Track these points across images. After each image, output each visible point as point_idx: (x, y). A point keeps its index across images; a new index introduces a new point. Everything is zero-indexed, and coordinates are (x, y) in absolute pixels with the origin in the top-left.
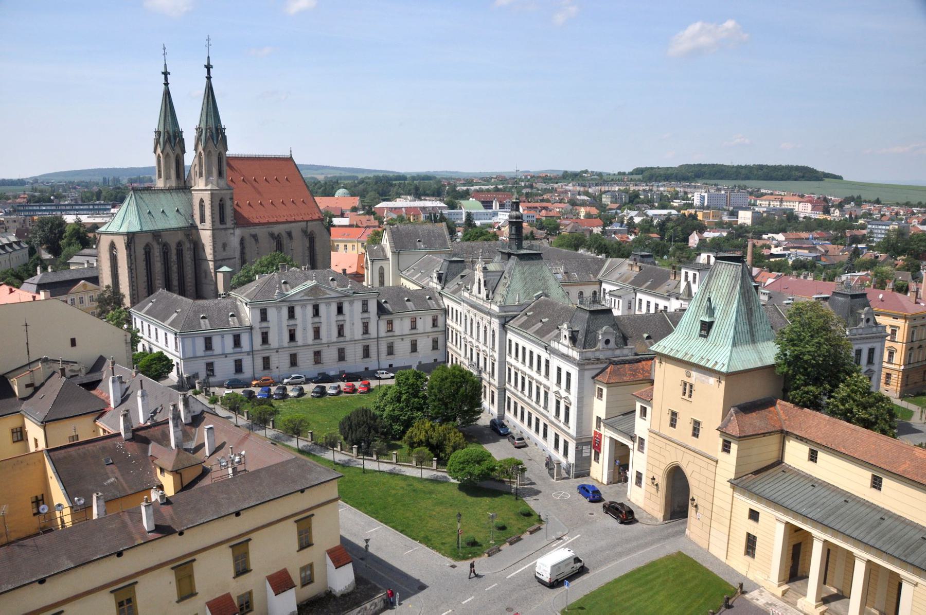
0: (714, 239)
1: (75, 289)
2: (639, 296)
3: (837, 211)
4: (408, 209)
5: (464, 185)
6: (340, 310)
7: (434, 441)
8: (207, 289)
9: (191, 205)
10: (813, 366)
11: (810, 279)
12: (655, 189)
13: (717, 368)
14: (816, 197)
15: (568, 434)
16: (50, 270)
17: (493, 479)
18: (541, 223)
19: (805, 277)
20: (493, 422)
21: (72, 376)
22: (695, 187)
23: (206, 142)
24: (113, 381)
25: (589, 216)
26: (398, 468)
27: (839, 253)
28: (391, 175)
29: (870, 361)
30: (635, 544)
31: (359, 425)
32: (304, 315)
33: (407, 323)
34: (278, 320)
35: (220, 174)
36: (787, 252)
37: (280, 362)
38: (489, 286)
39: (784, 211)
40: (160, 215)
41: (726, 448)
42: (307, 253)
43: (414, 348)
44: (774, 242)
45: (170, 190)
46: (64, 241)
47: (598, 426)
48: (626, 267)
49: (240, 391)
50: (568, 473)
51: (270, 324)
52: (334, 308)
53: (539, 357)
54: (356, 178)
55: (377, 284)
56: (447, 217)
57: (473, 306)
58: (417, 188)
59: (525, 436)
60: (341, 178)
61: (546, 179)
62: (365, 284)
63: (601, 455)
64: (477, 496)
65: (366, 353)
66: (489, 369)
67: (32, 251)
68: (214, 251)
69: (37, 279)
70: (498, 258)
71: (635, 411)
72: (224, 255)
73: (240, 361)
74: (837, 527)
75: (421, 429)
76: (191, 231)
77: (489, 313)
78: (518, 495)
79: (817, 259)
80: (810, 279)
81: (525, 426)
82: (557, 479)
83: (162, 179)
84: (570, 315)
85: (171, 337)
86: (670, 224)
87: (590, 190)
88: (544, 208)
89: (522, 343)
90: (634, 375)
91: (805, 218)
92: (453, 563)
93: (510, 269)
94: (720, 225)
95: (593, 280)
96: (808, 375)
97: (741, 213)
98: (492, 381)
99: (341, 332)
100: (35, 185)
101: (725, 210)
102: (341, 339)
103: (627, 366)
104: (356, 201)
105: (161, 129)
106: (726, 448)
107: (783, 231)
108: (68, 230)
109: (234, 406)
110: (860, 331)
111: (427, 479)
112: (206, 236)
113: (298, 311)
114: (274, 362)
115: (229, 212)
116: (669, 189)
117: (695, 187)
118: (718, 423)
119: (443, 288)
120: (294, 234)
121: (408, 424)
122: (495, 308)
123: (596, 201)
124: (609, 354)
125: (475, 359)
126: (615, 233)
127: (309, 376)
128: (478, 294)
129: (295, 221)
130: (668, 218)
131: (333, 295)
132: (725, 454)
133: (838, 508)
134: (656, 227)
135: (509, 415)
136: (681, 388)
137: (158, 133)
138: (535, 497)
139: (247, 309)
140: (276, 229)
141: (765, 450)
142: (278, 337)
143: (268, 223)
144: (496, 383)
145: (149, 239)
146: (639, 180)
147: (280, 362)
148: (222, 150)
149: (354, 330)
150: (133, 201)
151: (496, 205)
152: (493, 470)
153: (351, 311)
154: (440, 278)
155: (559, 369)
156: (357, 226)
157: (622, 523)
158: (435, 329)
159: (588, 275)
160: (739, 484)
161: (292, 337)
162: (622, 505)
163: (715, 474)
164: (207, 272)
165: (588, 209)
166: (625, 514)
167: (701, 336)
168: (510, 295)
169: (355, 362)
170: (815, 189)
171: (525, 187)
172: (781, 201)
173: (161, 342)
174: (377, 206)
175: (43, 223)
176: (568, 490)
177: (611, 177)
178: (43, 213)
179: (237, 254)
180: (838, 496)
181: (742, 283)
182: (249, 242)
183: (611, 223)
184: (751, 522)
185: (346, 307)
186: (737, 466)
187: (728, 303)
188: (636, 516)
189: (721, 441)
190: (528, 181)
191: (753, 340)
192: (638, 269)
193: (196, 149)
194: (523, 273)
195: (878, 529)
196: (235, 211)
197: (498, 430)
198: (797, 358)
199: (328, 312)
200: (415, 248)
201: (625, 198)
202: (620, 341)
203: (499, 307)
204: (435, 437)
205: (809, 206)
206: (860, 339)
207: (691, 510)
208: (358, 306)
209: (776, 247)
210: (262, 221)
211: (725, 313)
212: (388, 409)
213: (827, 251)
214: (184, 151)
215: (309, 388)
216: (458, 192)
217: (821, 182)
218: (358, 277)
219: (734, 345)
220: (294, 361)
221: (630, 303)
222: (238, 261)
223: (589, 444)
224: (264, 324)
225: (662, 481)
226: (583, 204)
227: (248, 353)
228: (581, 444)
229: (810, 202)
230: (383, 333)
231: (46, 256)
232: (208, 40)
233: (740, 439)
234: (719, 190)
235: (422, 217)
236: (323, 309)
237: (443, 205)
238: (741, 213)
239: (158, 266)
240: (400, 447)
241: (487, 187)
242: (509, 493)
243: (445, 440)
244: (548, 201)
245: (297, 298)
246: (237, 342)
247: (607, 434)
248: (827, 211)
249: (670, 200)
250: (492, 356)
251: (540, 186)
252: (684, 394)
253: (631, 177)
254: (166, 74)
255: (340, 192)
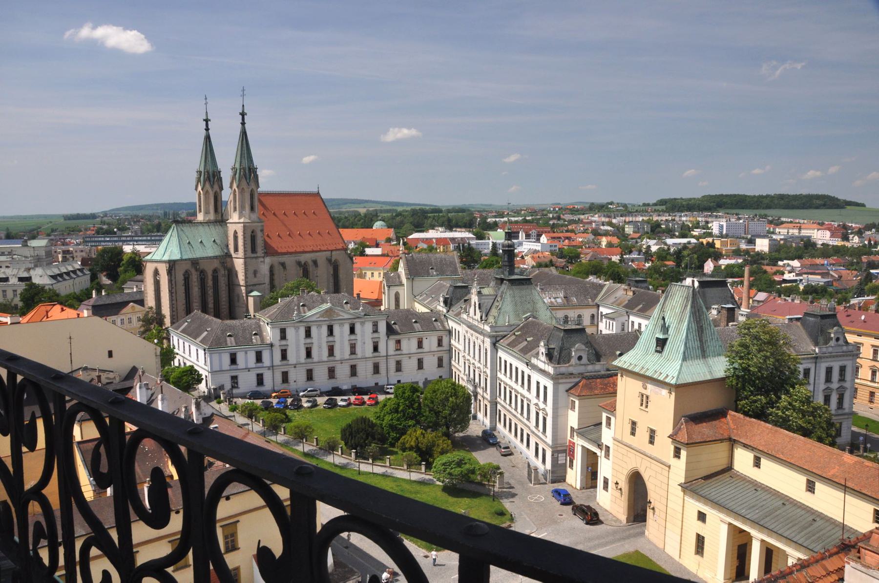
0: (728, 266)
1: (124, 311)
2: (632, 318)
3: (856, 237)
4: (439, 241)
5: (495, 217)
6: (352, 331)
7: (423, 447)
8: (239, 311)
9: (227, 237)
10: (758, 378)
11: (797, 301)
12: (677, 219)
13: (667, 380)
14: (836, 224)
15: (545, 442)
16: (103, 294)
17: (472, 482)
18: (562, 252)
19: (793, 300)
20: (484, 432)
21: (108, 383)
22: (716, 216)
23: (240, 180)
24: (140, 388)
25: (610, 245)
26: (390, 471)
27: (852, 278)
28: (427, 208)
29: (842, 378)
30: (596, 542)
31: (358, 432)
32: (319, 334)
33: (414, 343)
34: (295, 336)
35: (252, 208)
36: (798, 278)
37: (297, 377)
38: (484, 309)
39: (802, 238)
40: (199, 245)
41: (677, 454)
42: (332, 280)
43: (420, 363)
44: (789, 268)
45: (208, 223)
46: (122, 268)
47: (572, 436)
48: (623, 293)
49: (258, 402)
50: (546, 479)
51: (289, 343)
52: (347, 328)
53: (523, 372)
54: (396, 211)
55: (393, 307)
56: (474, 246)
57: (471, 327)
58: (449, 220)
59: (512, 445)
60: (381, 211)
61: (574, 211)
62: (383, 308)
63: (575, 462)
64: (457, 497)
65: (376, 369)
66: (483, 384)
67: (94, 277)
68: (246, 277)
69: (92, 302)
70: (492, 284)
71: (601, 423)
72: (255, 281)
73: (262, 375)
74: (770, 528)
75: (414, 435)
76: (226, 258)
77: (482, 333)
78: (496, 497)
79: (829, 284)
80: (797, 301)
81: (512, 436)
82: (535, 484)
83: (202, 213)
84: (548, 334)
85: (201, 352)
86: (685, 253)
87: (614, 221)
88: (567, 238)
89: (510, 360)
90: (605, 389)
91: (822, 245)
92: (427, 553)
93: (502, 292)
94: (737, 253)
95: (591, 303)
96: (754, 385)
97: (759, 241)
98: (485, 395)
99: (353, 351)
100: (105, 218)
101: (743, 238)
102: (353, 356)
103: (598, 380)
104: (391, 233)
105: (202, 169)
106: (677, 454)
107: (799, 258)
108: (125, 258)
109: (251, 413)
110: (830, 349)
111: (415, 481)
112: (239, 264)
113: (314, 331)
114: (292, 377)
115: (259, 242)
116: (691, 219)
117: (716, 216)
118: (670, 431)
119: (448, 311)
120: (319, 262)
121: (403, 432)
122: (487, 328)
123: (619, 231)
124: (581, 369)
125: (472, 376)
126: (633, 261)
127: (323, 390)
128: (474, 315)
129: (320, 251)
130: (685, 247)
131: (346, 316)
132: (676, 459)
133: (776, 509)
134: (673, 255)
135: (500, 426)
136: (639, 399)
137: (200, 173)
138: (511, 500)
139: (268, 328)
140: (303, 258)
141: (715, 456)
142: (296, 354)
143: (296, 253)
144: (488, 397)
145: (188, 266)
146: (663, 211)
147: (297, 377)
148: (253, 186)
149: (365, 349)
150: (175, 233)
151: (522, 235)
152: (473, 472)
153: (363, 332)
154: (446, 302)
155: (538, 383)
156: (388, 256)
157: (587, 524)
158: (441, 348)
159: (586, 299)
160: (690, 487)
161: (309, 354)
162: (589, 507)
163: (667, 478)
164: (239, 296)
165: (610, 238)
166: (591, 516)
167: (657, 351)
168: (501, 316)
169: (365, 378)
170: (835, 218)
171: (553, 218)
172: (800, 229)
173: (193, 358)
174: (410, 237)
175: (105, 251)
176: (543, 495)
177: (636, 208)
178: (107, 243)
179: (267, 280)
180: (778, 499)
181: (693, 302)
182: (278, 270)
183: (630, 252)
184: (700, 523)
185: (358, 328)
186: (687, 471)
187: (681, 321)
188: (601, 518)
189: (672, 448)
190: (557, 212)
191: (704, 354)
192: (631, 294)
193: (231, 187)
194: (514, 297)
195: (809, 529)
196: (266, 243)
197: (488, 439)
198: (746, 370)
199: (341, 332)
200: (428, 275)
201: (647, 228)
202: (593, 358)
203: (491, 327)
204: (424, 442)
205: (828, 233)
206: (830, 357)
207: (650, 513)
208: (369, 327)
209: (790, 272)
210: (290, 250)
211: (678, 330)
212: (388, 418)
213: (840, 277)
214: (221, 188)
215: (321, 400)
216: (489, 224)
217: (843, 211)
218: (378, 302)
219: (684, 359)
220: (310, 376)
221: (623, 325)
222: (267, 286)
223: (562, 451)
224: (284, 342)
225: (624, 485)
226: (606, 234)
227: (269, 368)
228: (555, 452)
229: (829, 229)
230: (391, 351)
231: (106, 281)
232: (243, 90)
233: (688, 445)
234: (739, 219)
235: (452, 247)
236: (336, 329)
237: (471, 235)
238: (759, 241)
239: (195, 291)
240: (396, 453)
241: (516, 219)
242: (488, 495)
243: (434, 446)
244: (572, 231)
245: (314, 319)
246: (259, 358)
247: (580, 443)
248: (845, 238)
249: (690, 229)
250: (485, 372)
251: (568, 217)
252: (642, 405)
253: (654, 207)
254: (243, 114)
255: (378, 225)
